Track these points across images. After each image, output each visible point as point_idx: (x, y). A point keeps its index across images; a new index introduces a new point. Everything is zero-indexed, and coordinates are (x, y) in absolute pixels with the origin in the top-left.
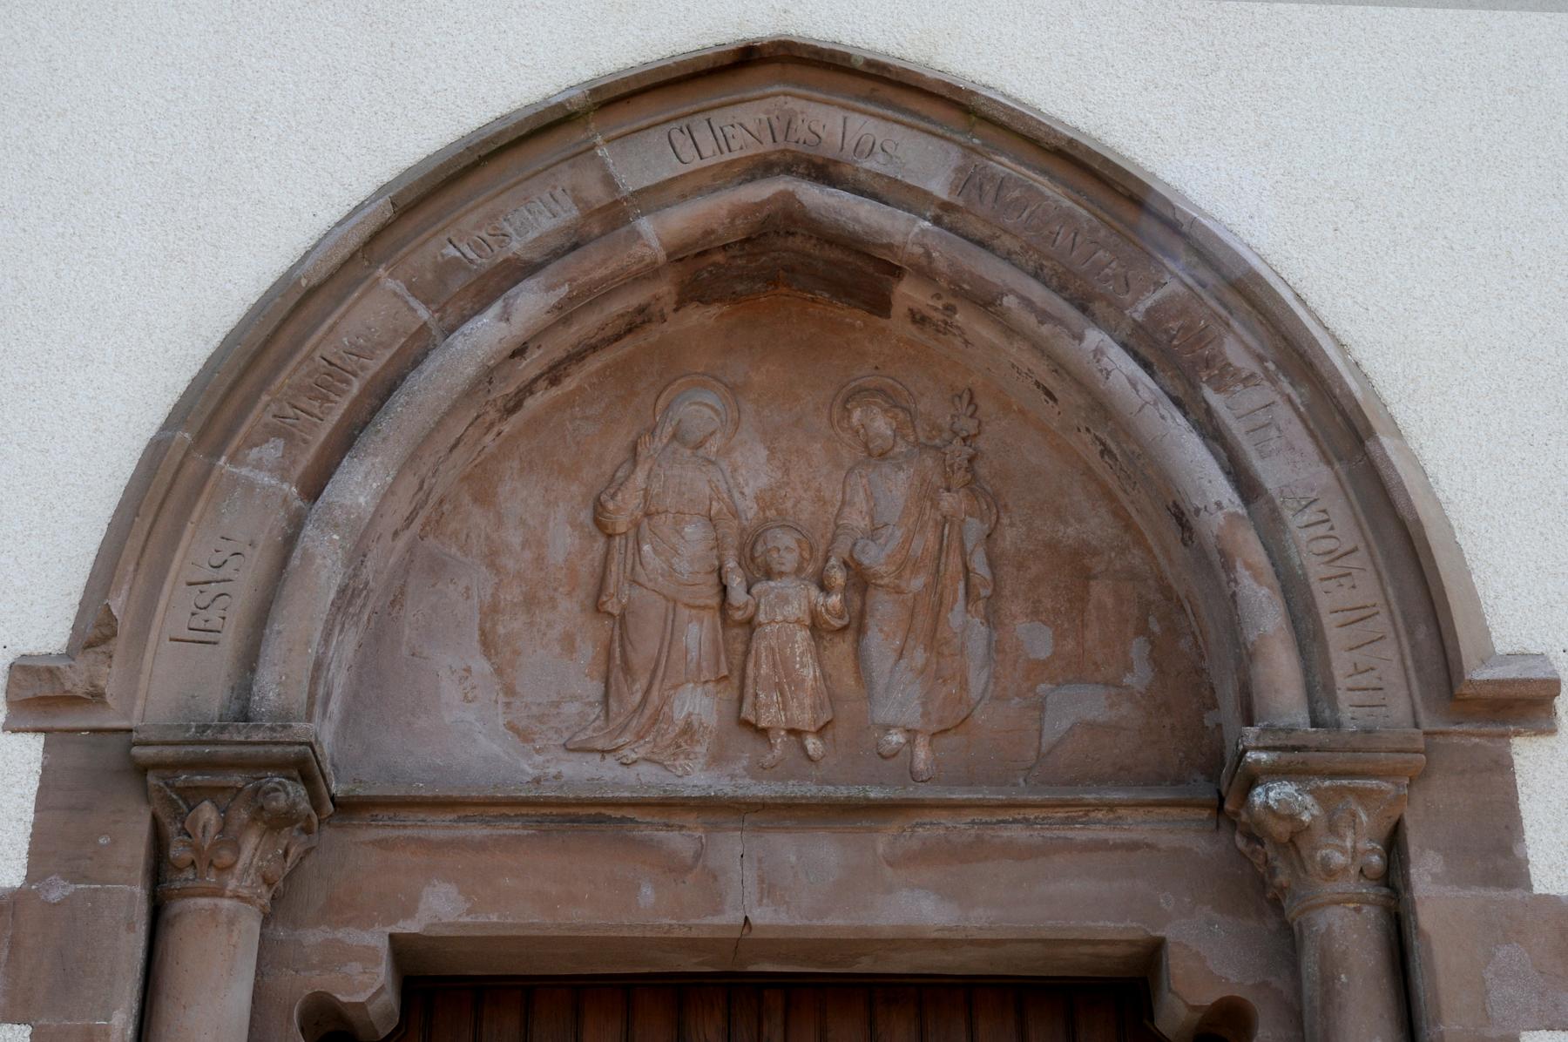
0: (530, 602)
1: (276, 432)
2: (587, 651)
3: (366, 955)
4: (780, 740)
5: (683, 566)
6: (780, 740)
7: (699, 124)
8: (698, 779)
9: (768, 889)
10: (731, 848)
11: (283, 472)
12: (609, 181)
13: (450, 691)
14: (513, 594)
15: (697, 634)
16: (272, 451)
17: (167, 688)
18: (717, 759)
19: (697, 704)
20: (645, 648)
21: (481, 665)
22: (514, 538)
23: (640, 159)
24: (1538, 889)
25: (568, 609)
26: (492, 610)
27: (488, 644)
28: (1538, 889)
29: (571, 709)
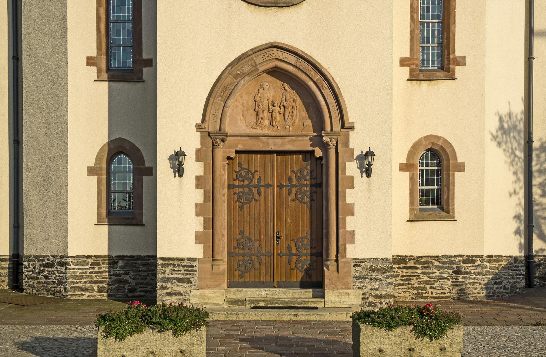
0: (247, 110)
1: (220, 96)
2: (254, 116)
3: (233, 152)
4: (276, 127)
5: (264, 106)
6: (276, 127)
7: (265, 54)
8: (266, 132)
9: (274, 145)
10: (270, 140)
11: (221, 101)
12: (255, 62)
13: (239, 121)
14: (245, 109)
15: (266, 114)
16: (220, 98)
17: (212, 127)
18: (268, 129)
19: (267, 123)
20: (260, 116)
21: (242, 118)
22: (245, 102)
23: (259, 59)
24: (347, 175)
25: (252, 111)
26: (243, 111)
27: (243, 115)
28: (347, 175)
29: (252, 123)
